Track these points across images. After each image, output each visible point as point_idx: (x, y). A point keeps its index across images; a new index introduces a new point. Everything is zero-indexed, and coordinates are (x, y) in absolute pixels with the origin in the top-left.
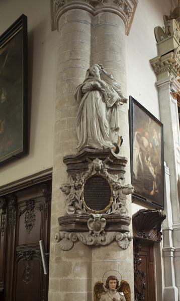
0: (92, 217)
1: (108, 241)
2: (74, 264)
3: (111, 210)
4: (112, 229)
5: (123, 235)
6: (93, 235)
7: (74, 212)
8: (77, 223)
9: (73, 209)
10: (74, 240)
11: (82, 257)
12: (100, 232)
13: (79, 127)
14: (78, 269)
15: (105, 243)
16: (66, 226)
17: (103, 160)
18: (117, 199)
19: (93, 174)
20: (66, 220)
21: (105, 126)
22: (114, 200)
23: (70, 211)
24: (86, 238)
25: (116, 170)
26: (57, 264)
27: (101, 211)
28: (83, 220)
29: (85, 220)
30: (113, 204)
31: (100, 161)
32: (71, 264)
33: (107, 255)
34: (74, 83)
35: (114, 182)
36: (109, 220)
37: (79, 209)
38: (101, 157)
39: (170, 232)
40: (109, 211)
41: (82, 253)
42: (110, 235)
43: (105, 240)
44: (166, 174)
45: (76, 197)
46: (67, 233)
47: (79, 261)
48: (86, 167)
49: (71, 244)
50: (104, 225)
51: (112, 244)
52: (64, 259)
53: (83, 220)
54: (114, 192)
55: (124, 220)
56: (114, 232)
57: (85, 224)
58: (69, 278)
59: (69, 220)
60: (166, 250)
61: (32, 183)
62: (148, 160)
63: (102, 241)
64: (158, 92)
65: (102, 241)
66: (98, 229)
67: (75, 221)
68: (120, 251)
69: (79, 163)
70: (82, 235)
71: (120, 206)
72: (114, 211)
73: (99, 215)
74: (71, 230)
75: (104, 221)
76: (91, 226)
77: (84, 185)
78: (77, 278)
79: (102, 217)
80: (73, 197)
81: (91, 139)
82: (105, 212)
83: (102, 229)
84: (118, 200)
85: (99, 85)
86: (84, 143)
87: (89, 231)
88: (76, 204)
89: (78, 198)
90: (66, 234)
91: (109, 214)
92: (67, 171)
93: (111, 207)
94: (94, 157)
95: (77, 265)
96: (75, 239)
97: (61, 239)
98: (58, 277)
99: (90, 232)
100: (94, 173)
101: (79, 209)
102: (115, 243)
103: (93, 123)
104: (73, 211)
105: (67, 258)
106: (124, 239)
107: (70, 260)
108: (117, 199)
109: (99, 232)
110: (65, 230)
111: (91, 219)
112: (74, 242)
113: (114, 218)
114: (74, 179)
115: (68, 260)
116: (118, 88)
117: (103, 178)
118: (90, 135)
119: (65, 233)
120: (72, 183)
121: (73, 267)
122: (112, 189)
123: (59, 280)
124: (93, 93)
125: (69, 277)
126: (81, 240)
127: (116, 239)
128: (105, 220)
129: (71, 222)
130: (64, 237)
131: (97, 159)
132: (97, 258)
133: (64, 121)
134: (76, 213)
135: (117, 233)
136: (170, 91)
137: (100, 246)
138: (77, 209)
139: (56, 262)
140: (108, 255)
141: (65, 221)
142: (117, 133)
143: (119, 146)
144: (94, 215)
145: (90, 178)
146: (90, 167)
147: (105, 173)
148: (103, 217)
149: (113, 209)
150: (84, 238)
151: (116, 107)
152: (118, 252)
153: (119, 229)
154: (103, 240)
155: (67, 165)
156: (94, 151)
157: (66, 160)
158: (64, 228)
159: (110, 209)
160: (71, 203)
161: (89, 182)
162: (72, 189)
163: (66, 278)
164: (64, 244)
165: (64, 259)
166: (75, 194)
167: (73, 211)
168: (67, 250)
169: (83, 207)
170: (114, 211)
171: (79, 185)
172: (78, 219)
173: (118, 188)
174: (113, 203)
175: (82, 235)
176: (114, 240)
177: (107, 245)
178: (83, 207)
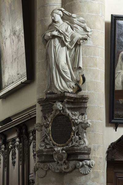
1: (70, 169)
5: (81, 163)
6: (59, 164)
7: (44, 147)
8: (46, 156)
10: (46, 169)
15: (67, 171)
17: (62, 102)
19: (57, 114)
25: (77, 107)
28: (49, 153)
29: (51, 153)
33: (71, 180)
35: (73, 119)
38: (60, 100)
40: (71, 144)
41: (53, 179)
42: (72, 164)
43: (68, 168)
46: (41, 164)
49: (44, 173)
50: (65, 156)
51: (75, 171)
53: (49, 153)
54: (73, 128)
55: (79, 151)
56: (74, 161)
57: (52, 156)
61: (30, 116)
66: (61, 160)
68: (81, 176)
69: (48, 104)
70: (51, 165)
71: (80, 139)
72: (74, 143)
73: (59, 148)
74: (42, 161)
76: (55, 158)
77: (51, 124)
79: (62, 150)
80: (44, 134)
82: (67, 145)
83: (64, 160)
84: (78, 134)
88: (46, 141)
91: (70, 146)
92: (41, 111)
93: (72, 140)
94: (55, 101)
96: (47, 168)
102: (77, 170)
103: (52, 72)
104: (43, 146)
106: (83, 166)
109: (62, 162)
112: (46, 171)
116: (83, 23)
122: (72, 125)
126: (51, 169)
127: (77, 167)
130: (39, 168)
135: (77, 161)
137: (65, 173)
140: (72, 180)
141: (40, 154)
143: (80, 84)
145: (55, 117)
148: (64, 150)
149: (73, 141)
150: (53, 167)
151: (80, 45)
152: (79, 177)
153: (76, 158)
154: (65, 168)
156: (54, 96)
159: (71, 142)
161: (54, 121)
164: (42, 173)
167: (43, 146)
168: (42, 178)
171: (47, 124)
173: (76, 124)
175: (51, 165)
176: (75, 168)
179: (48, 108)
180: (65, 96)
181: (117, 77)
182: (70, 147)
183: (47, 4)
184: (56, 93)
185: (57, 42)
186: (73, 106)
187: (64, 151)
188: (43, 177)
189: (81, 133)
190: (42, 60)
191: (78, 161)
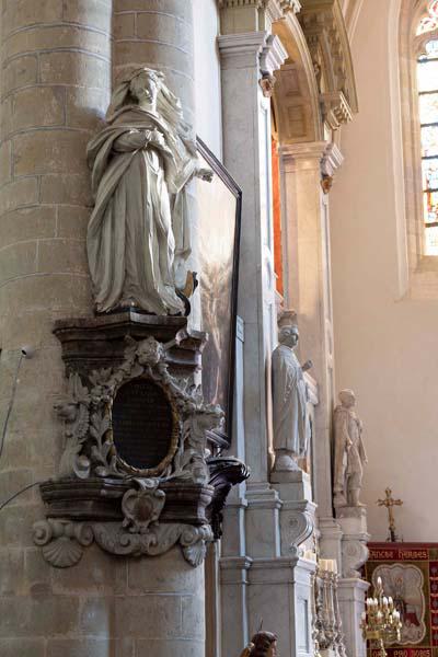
0: (137, 486)
2: (82, 602)
3: (173, 470)
4: (177, 517)
6: (132, 530)
9: (87, 463)
11: (99, 584)
12: (149, 521)
13: (96, 242)
14: (92, 615)
16: (67, 506)
18: (186, 441)
20: (73, 491)
21: (170, 250)
22: (179, 445)
23: (81, 468)
24: (108, 533)
26: (37, 603)
27: (152, 470)
28: (113, 492)
30: (179, 453)
31: (159, 346)
32: (75, 602)
34: (76, 103)
35: (181, 397)
36: (171, 495)
37: (101, 463)
39: (242, 512)
41: (98, 573)
42: (170, 532)
44: (237, 340)
45: (94, 431)
47: (95, 594)
48: (117, 353)
50: (159, 506)
52: (57, 589)
58: (72, 638)
59: (81, 491)
60: (230, 564)
62: (212, 311)
63: (151, 544)
64: (222, 69)
65: (151, 544)
67: (98, 495)
75: (160, 498)
76: (129, 509)
78: (91, 636)
81: (137, 284)
85: (161, 141)
86: (117, 292)
87: (122, 519)
89: (98, 436)
90: (67, 527)
91: (167, 478)
93: (172, 463)
94: (143, 335)
95: (89, 603)
97: (53, 538)
98: (40, 635)
99: (125, 523)
100: (139, 372)
101: (101, 463)
104: (86, 469)
105: (65, 586)
107: (73, 592)
108: (186, 441)
109: (146, 524)
110: (66, 516)
111: (132, 492)
113: (183, 491)
114: (86, 382)
115: (67, 593)
117: (157, 386)
118: (134, 272)
119: (64, 524)
120: (83, 394)
121: (80, 610)
123: (46, 642)
124: (146, 155)
125: (71, 635)
128: (164, 494)
129: (86, 497)
130: (62, 535)
131: (151, 339)
132: (132, 587)
133: (48, 213)
134: (93, 473)
135: (184, 526)
136: (259, 76)
137: (146, 556)
138: (95, 464)
139: (35, 597)
140: (161, 580)
142: (182, 261)
144: (142, 482)
146: (130, 358)
147: (162, 375)
155: (63, 343)
157: (62, 331)
158: (63, 511)
159: (170, 467)
160: (79, 448)
161: (127, 391)
162: (83, 410)
163: (64, 638)
165: (57, 589)
166: (91, 423)
167: (86, 469)
169: (109, 459)
170: (180, 472)
172: (104, 492)
174: (177, 451)
177: (158, 556)
178: (109, 459)
179: (96, 353)
180: (130, 321)
181: (229, 264)
182: (169, 480)
183: (79, 48)
184: (153, 314)
185: (153, 162)
186: (173, 357)
187: (162, 493)
188: (67, 563)
189: (197, 442)
190: (63, 205)
191: (89, 524)
